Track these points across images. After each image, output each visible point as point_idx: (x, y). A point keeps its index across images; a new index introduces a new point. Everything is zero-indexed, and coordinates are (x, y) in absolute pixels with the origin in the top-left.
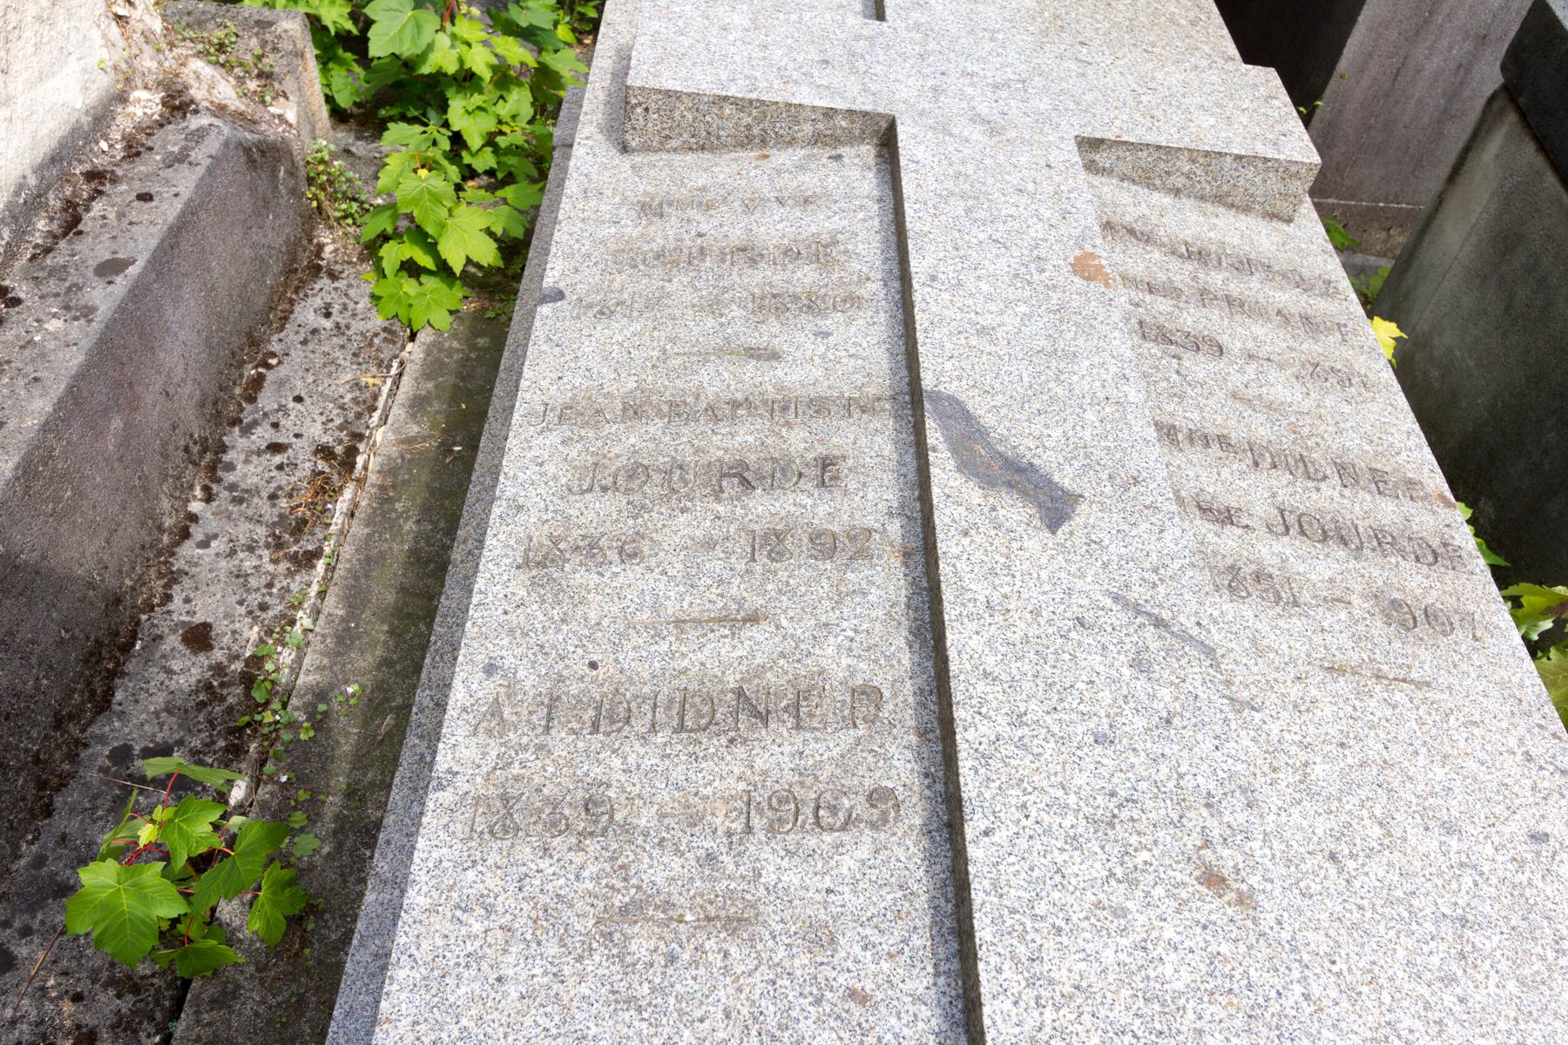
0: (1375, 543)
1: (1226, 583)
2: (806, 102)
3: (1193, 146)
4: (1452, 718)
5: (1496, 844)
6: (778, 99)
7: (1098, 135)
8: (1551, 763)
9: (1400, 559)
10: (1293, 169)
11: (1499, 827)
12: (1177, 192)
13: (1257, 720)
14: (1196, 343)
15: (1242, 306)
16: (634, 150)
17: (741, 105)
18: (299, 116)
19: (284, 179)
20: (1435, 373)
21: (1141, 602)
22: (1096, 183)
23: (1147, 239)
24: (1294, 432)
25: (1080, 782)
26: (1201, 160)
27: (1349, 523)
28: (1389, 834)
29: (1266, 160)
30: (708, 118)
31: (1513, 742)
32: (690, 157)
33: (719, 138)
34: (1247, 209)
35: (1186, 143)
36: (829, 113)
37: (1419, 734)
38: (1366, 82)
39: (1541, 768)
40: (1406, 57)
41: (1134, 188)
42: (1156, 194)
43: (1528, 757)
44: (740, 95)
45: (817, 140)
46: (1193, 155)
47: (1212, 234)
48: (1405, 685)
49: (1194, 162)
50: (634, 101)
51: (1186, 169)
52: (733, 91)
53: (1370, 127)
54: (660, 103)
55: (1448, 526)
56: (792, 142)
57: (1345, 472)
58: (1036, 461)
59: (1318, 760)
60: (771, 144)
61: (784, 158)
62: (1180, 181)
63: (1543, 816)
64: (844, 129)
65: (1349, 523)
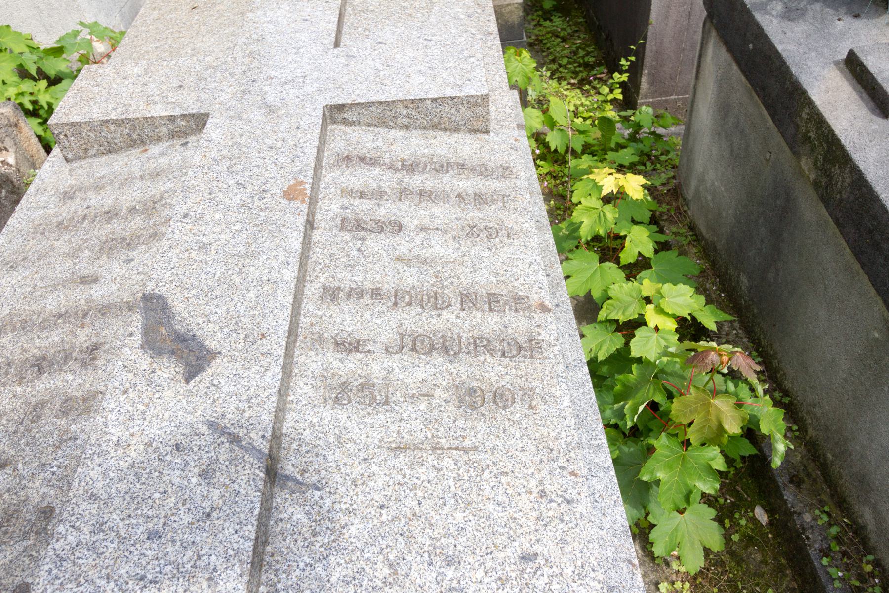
0: (472, 348)
1: (334, 396)
2: (155, 115)
3: (403, 98)
4: (486, 473)
5: (488, 568)
6: (139, 116)
7: (340, 102)
8: (561, 496)
9: (488, 356)
10: (472, 100)
11: (496, 554)
12: (407, 127)
13: (316, 498)
14: (380, 227)
15: (429, 196)
16: (72, 160)
17: (120, 123)
18: (16, 158)
19: (6, 197)
20: (709, 198)
21: (228, 426)
22: (349, 131)
23: (374, 162)
24: (437, 277)
25: (123, 571)
26: (412, 106)
27: (455, 336)
28: (395, 573)
29: (452, 98)
30: (103, 134)
31: (533, 483)
32: (104, 159)
33: (116, 144)
34: (456, 130)
35: (401, 97)
36: (172, 118)
37: (453, 488)
38: (671, 23)
39: (551, 501)
40: (692, 4)
41: (376, 130)
42: (393, 131)
43: (543, 493)
44: (115, 118)
45: (172, 135)
46: (406, 104)
47: (426, 151)
48: (455, 452)
49: (407, 107)
50: (56, 132)
51: (405, 112)
52: (113, 116)
53: (683, 50)
54: (71, 130)
55: (538, 326)
56: (159, 139)
57: (467, 300)
58: (198, 333)
59: (356, 521)
60: (148, 142)
61: (155, 150)
62: (406, 121)
63: (538, 540)
64: (185, 126)
65: (455, 336)
